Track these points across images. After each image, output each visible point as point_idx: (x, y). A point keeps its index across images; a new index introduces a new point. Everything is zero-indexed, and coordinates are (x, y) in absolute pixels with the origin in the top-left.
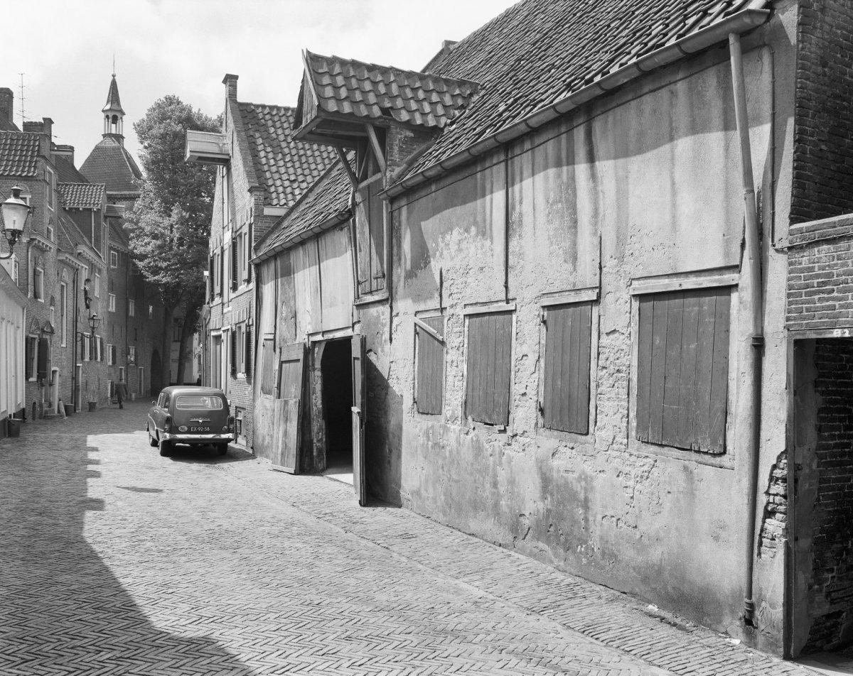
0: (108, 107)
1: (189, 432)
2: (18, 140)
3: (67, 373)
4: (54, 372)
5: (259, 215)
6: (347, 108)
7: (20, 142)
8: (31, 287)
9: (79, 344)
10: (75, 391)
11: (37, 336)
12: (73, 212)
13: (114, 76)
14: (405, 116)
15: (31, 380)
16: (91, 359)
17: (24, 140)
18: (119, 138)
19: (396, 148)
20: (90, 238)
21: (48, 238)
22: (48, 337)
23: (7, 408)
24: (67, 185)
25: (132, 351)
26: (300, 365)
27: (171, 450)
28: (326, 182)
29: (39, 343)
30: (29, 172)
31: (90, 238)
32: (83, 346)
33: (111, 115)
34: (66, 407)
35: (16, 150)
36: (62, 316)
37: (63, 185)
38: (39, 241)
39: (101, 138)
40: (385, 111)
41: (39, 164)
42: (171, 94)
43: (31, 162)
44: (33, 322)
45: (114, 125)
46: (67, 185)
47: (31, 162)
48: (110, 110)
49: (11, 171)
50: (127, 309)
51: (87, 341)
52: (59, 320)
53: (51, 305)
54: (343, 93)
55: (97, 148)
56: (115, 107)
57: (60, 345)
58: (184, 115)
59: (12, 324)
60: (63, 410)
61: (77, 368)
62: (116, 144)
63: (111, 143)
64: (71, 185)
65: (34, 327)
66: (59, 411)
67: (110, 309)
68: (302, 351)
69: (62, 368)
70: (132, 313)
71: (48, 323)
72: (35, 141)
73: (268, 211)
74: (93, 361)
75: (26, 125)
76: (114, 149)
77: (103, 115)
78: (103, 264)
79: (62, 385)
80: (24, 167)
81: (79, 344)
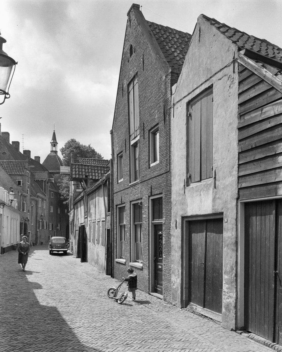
0: (52, 141)
1: (56, 248)
2: (19, 163)
3: (34, 233)
4: (29, 233)
5: (75, 191)
6: (77, 176)
7: (19, 164)
8: (22, 208)
9: (38, 224)
10: (37, 238)
11: (24, 222)
12: (38, 181)
13: (54, 131)
14: (91, 177)
15: (22, 235)
16: (42, 228)
17: (20, 163)
18: (56, 152)
19: (89, 184)
20: (43, 189)
21: (27, 193)
22: (27, 222)
23: (13, 242)
24: (36, 172)
25: (59, 225)
26: (78, 231)
27: (52, 253)
28: (137, 162)
29: (24, 224)
30: (22, 173)
31: (43, 189)
32: (39, 225)
33: (53, 144)
34: (33, 243)
35: (16, 170)
36: (32, 215)
37: (34, 172)
38: (24, 194)
39: (50, 152)
40: (86, 176)
41: (24, 171)
42: (73, 138)
43: (22, 170)
44: (22, 218)
45: (54, 148)
46: (36, 172)
47: (22, 170)
48: (53, 142)
49: (15, 173)
50: (57, 211)
51: (41, 223)
52: (31, 217)
53: (28, 212)
54: (77, 173)
55: (49, 156)
56: (55, 142)
57: (31, 225)
58: (77, 146)
59: (15, 219)
60: (32, 244)
61: (37, 231)
62: (55, 154)
63: (53, 154)
64: (37, 172)
65: (23, 219)
66: (31, 244)
67: (51, 212)
68: (78, 228)
69: (32, 231)
70: (59, 212)
71: (27, 218)
72: (24, 163)
73: (78, 190)
74: (43, 229)
75: (24, 151)
76: (54, 156)
77: (50, 144)
78: (47, 198)
79: (32, 237)
80: (20, 172)
81: (38, 224)
